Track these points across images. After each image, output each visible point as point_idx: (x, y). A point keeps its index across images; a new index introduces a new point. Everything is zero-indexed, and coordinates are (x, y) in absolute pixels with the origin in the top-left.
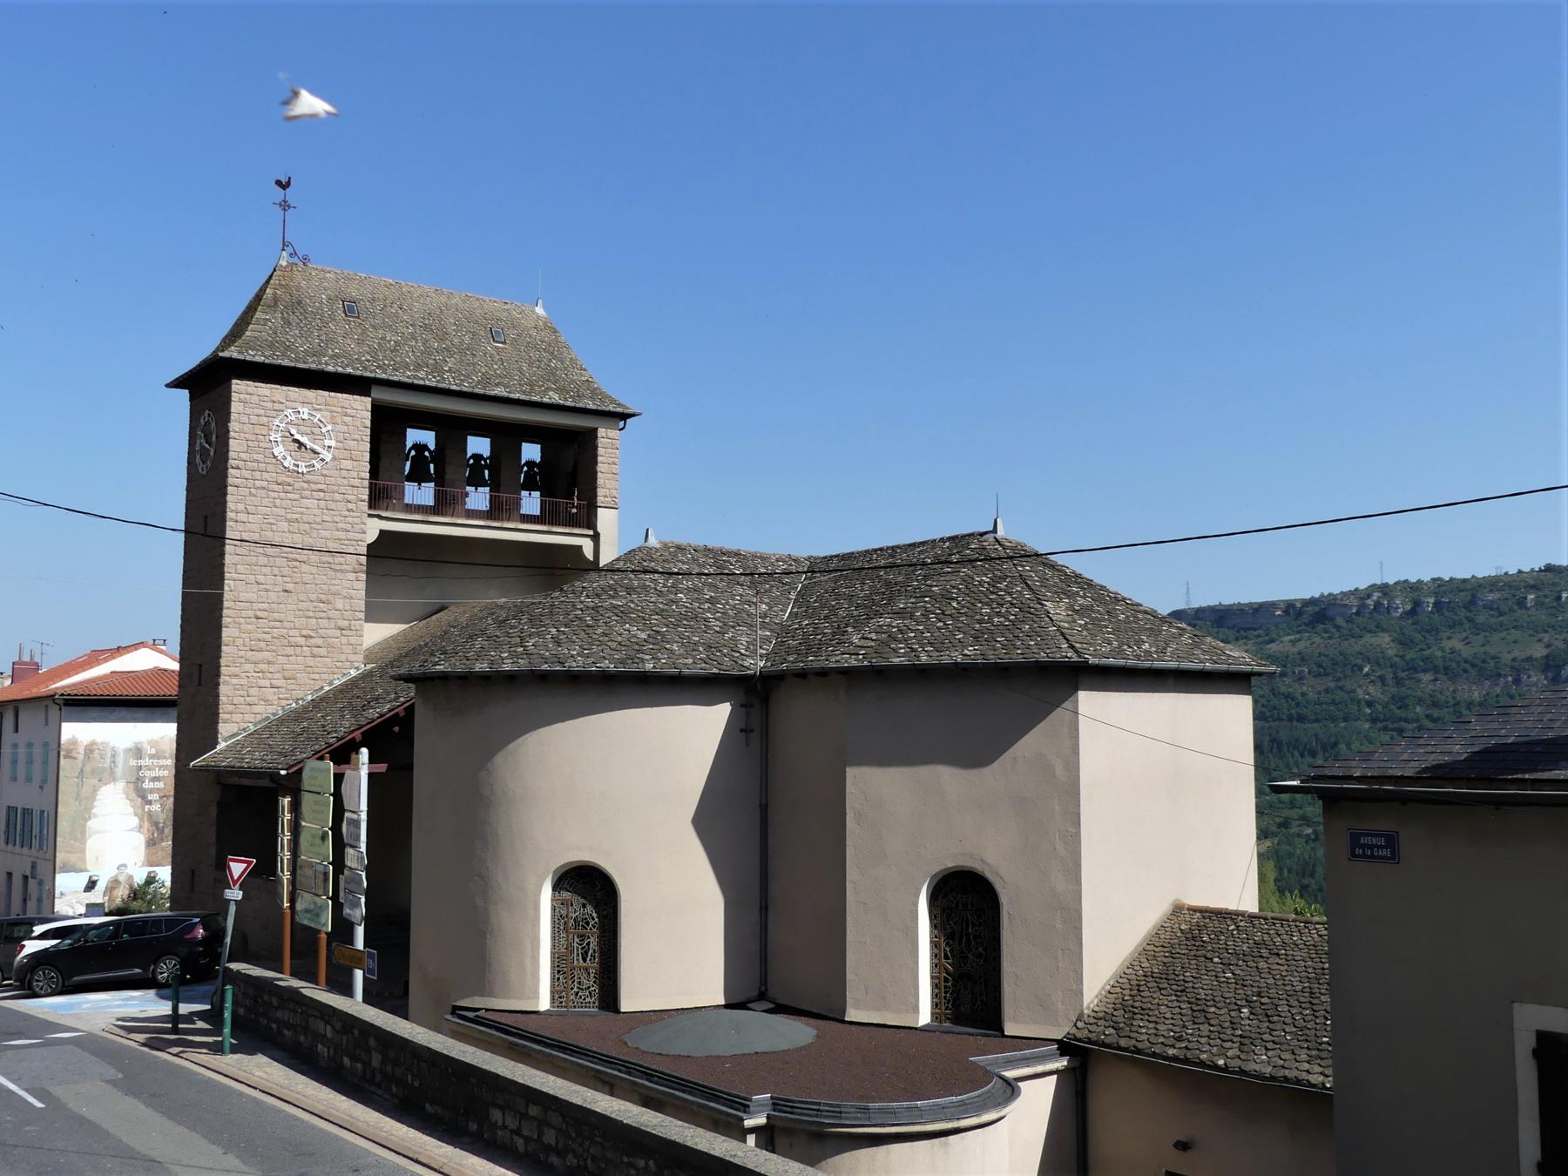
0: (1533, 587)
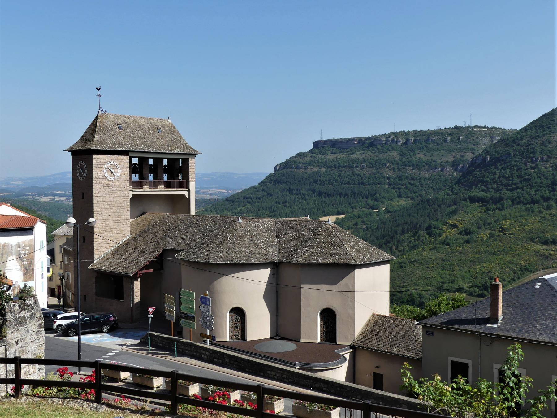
0: (450, 134)
